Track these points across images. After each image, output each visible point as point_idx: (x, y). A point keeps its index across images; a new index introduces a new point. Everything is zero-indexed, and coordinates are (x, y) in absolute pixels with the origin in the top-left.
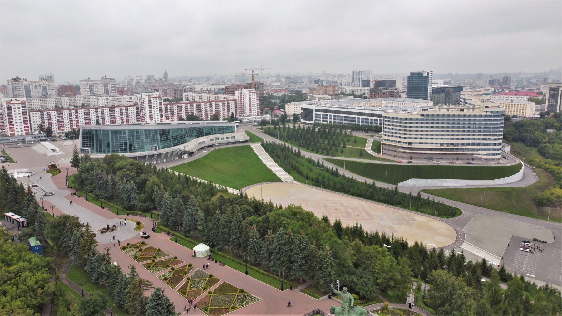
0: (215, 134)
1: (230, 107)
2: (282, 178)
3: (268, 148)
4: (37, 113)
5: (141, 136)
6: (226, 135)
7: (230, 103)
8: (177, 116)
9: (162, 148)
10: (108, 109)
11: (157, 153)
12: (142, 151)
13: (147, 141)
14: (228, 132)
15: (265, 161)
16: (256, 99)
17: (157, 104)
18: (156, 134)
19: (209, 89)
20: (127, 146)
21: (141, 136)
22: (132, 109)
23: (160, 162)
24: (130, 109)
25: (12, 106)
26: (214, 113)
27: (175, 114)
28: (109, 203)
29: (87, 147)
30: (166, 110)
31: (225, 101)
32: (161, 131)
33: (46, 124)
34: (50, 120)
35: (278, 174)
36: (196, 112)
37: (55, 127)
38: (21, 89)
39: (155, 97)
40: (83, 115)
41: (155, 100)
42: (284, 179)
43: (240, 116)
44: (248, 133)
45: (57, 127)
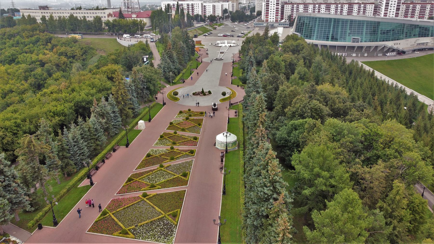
4: (289, 5)
9: (365, 41)
11: (357, 46)
12: (344, 42)
13: (351, 31)
22: (371, 7)
24: (368, 6)
30: (406, 9)
32: (368, 23)
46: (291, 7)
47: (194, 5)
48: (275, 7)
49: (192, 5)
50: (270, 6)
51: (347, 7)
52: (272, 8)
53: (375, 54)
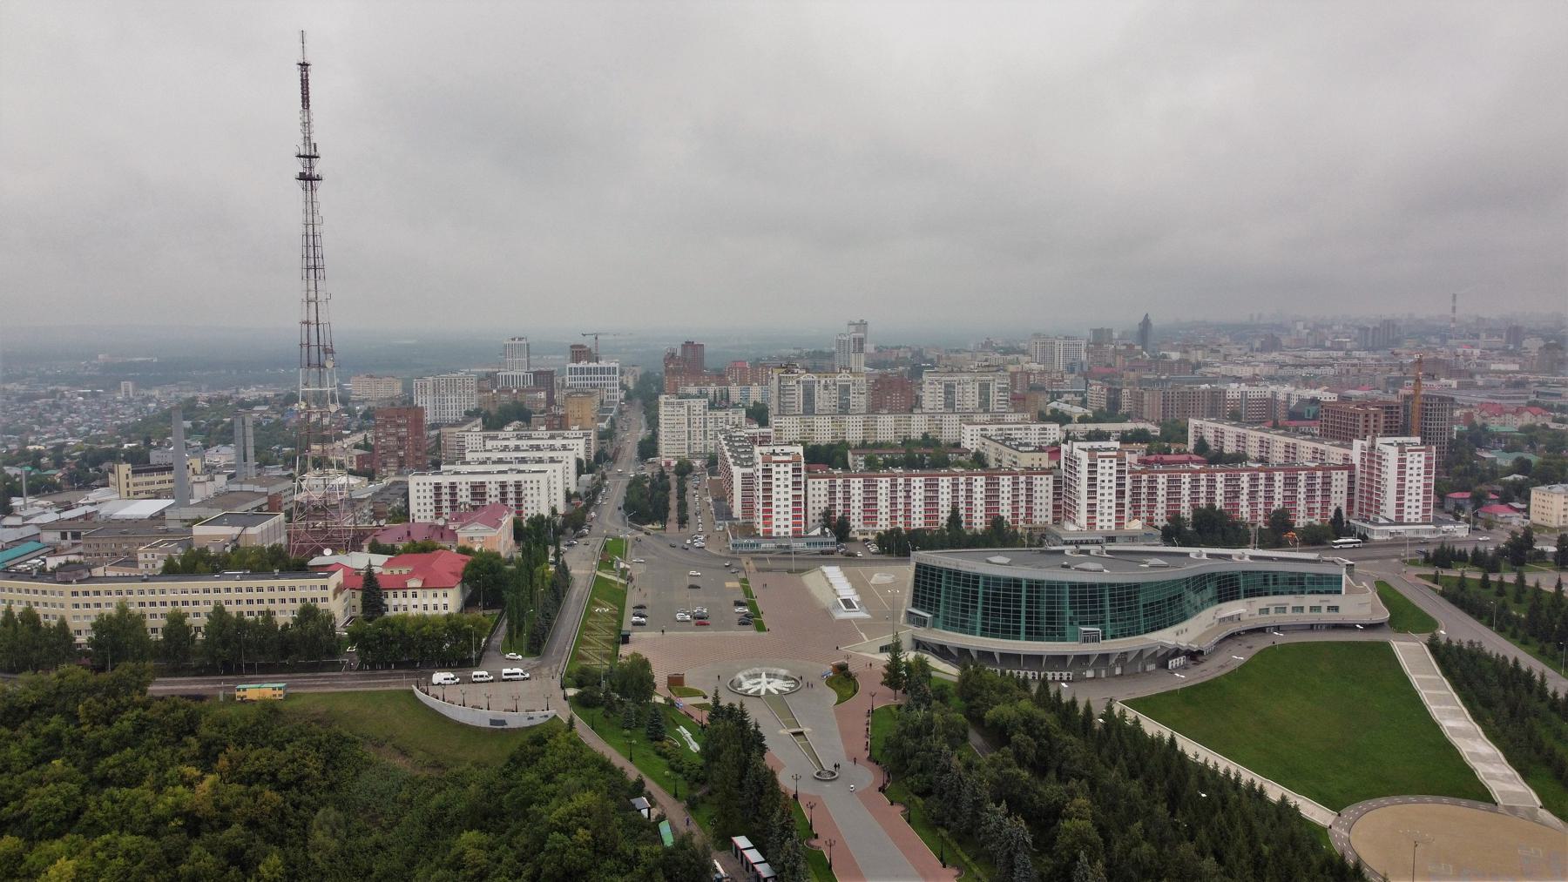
0: (1275, 593)
1: (1333, 489)
2: (1495, 787)
3: (1454, 662)
4: (823, 481)
5: (1058, 603)
6: (1310, 600)
7: (1334, 477)
8: (1164, 505)
10: (984, 477)
13: (1075, 613)
14: (1318, 592)
15: (1438, 711)
16: (1422, 471)
17: (1111, 475)
18: (1101, 596)
19: (1269, 395)
20: (1020, 622)
21: (1058, 597)
22: (1044, 482)
23: (1103, 673)
25: (774, 466)
26: (1278, 503)
27: (1160, 499)
28: (959, 850)
29: (922, 608)
31: (1315, 469)
32: (1114, 589)
33: (838, 508)
34: (847, 498)
35: (1482, 770)
36: (1222, 498)
37: (855, 517)
38: (796, 392)
39: (1107, 457)
40: (922, 490)
41: (1107, 464)
42: (1502, 793)
43: (1364, 521)
44: (1386, 594)
45: (861, 517)
46: (827, 486)
47: (524, 486)
48: (791, 493)
49: (518, 485)
50: (775, 489)
51: (983, 483)
52: (782, 496)
53: (1140, 667)
